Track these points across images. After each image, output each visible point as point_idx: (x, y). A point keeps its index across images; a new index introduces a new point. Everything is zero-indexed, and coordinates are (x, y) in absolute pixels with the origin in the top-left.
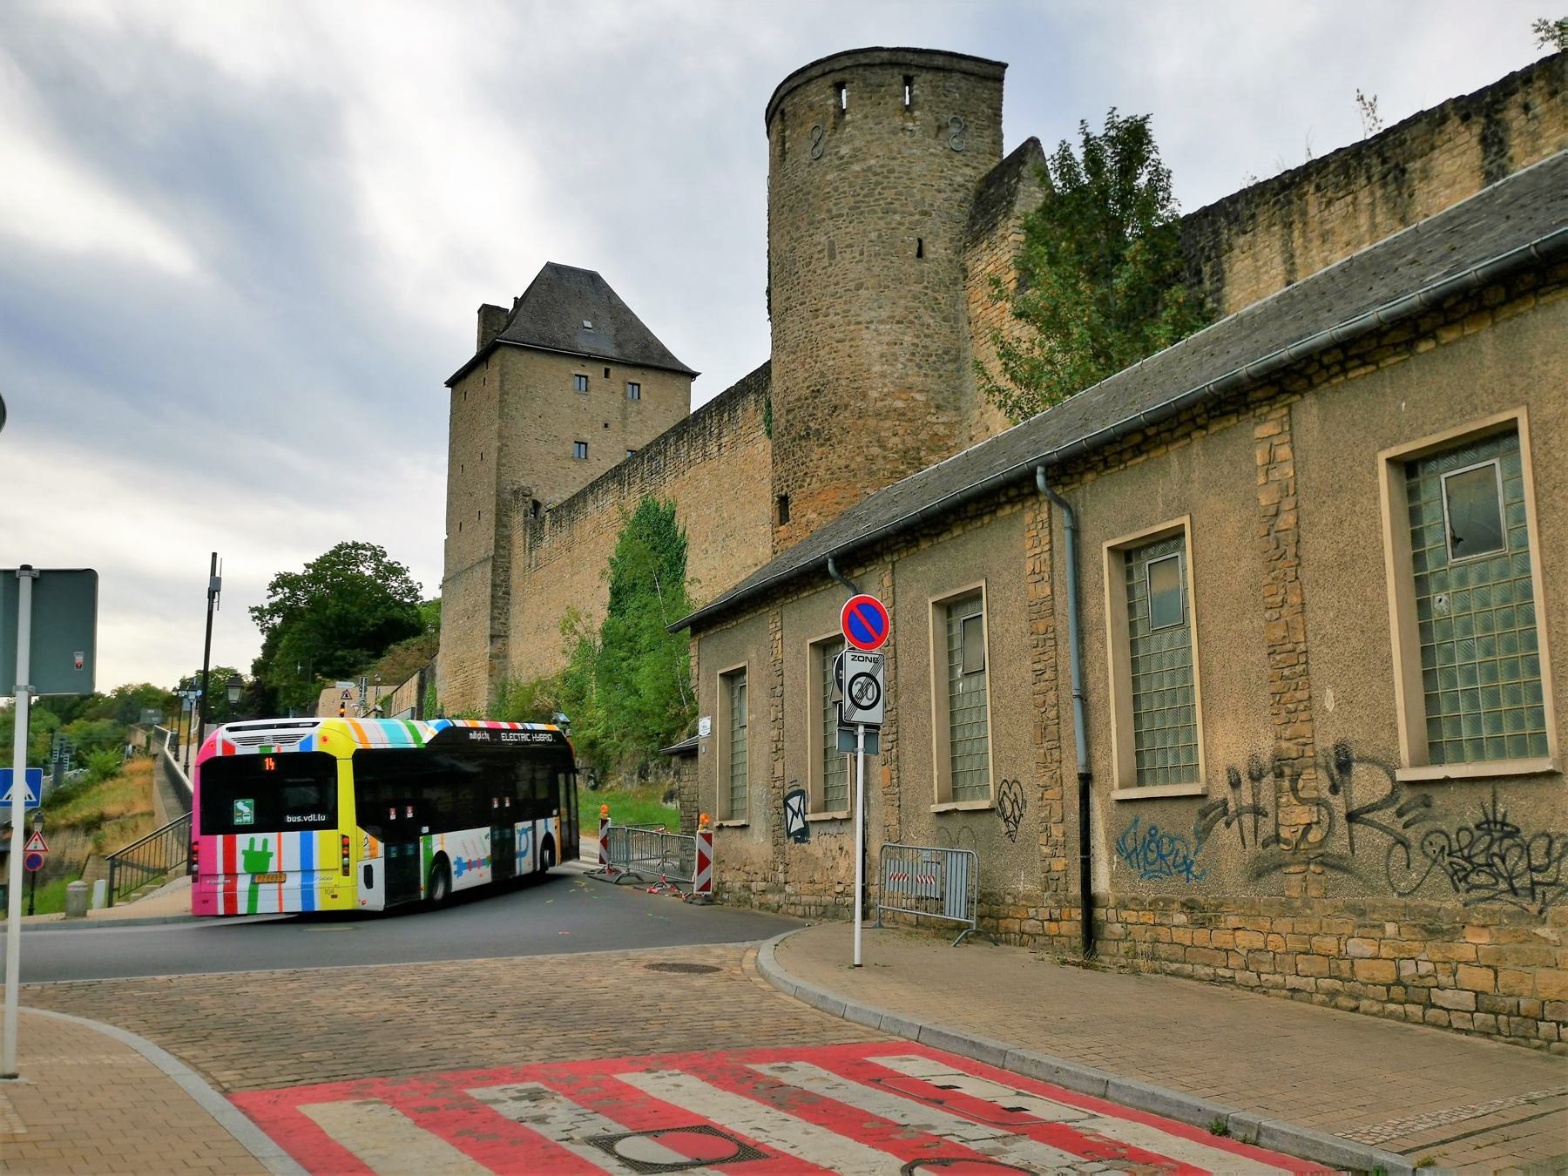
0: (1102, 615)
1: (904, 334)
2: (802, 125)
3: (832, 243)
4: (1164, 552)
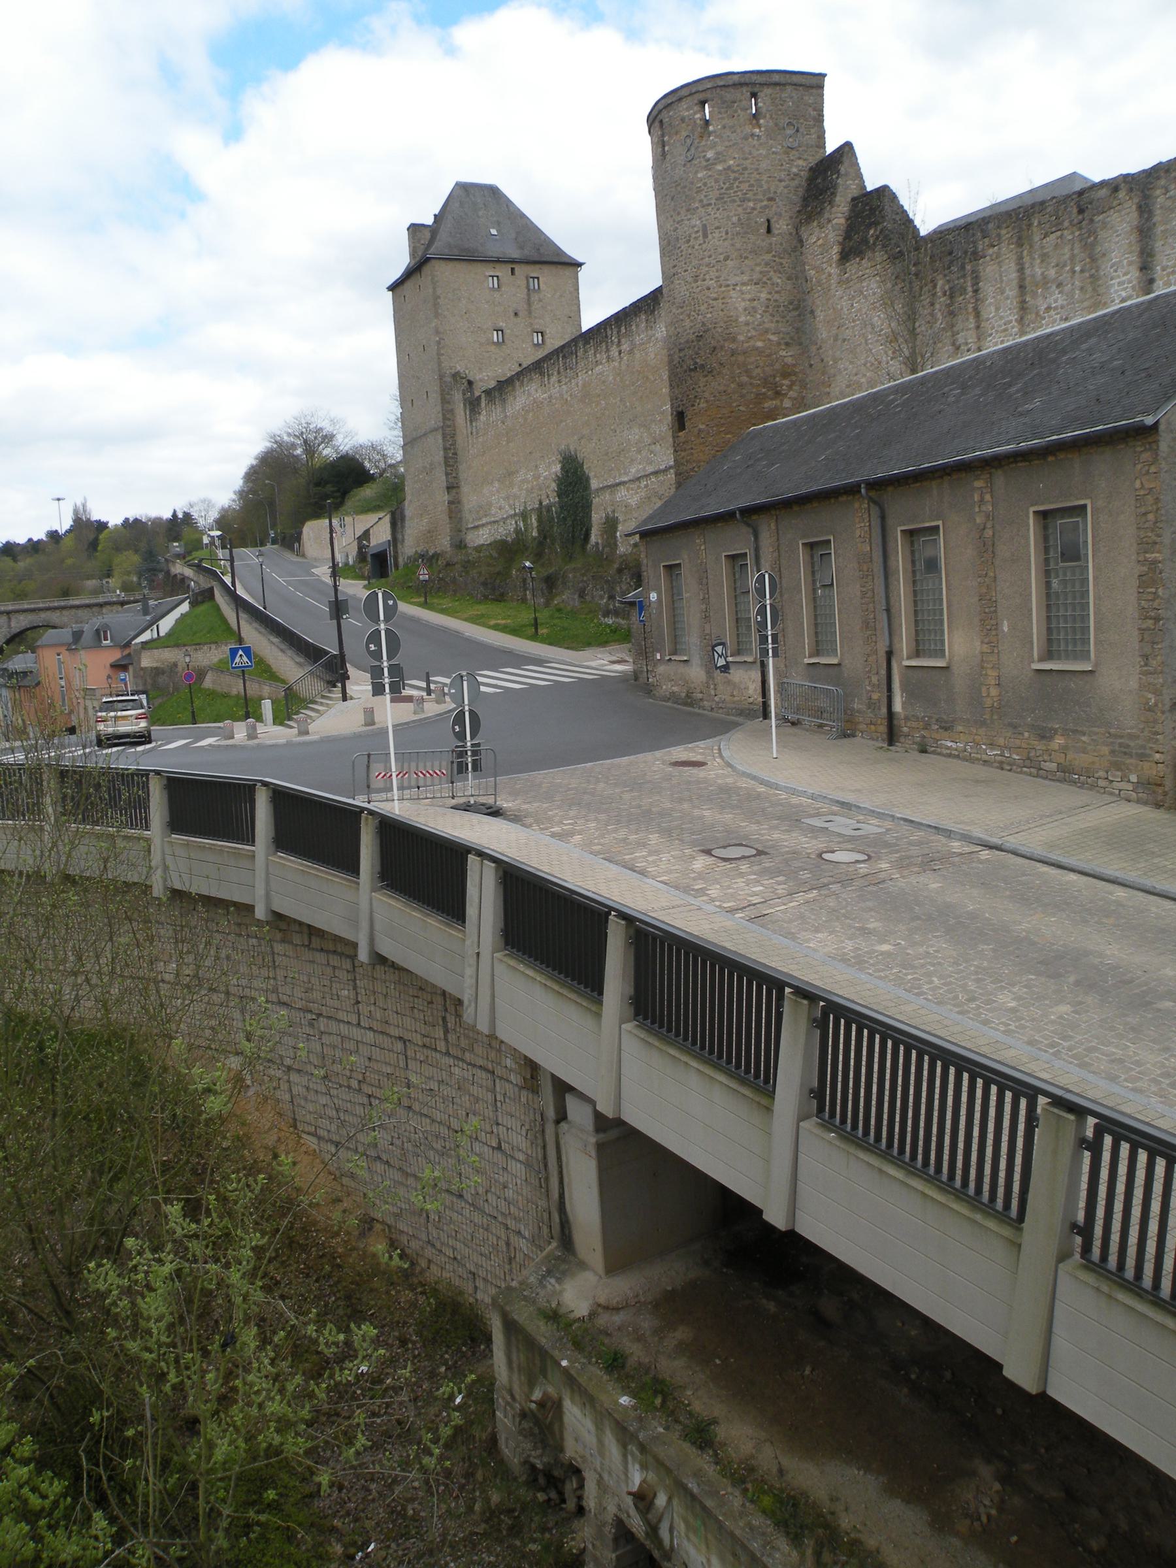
0: (898, 566)
1: (761, 292)
2: (677, 133)
3: (704, 227)
4: (931, 535)
